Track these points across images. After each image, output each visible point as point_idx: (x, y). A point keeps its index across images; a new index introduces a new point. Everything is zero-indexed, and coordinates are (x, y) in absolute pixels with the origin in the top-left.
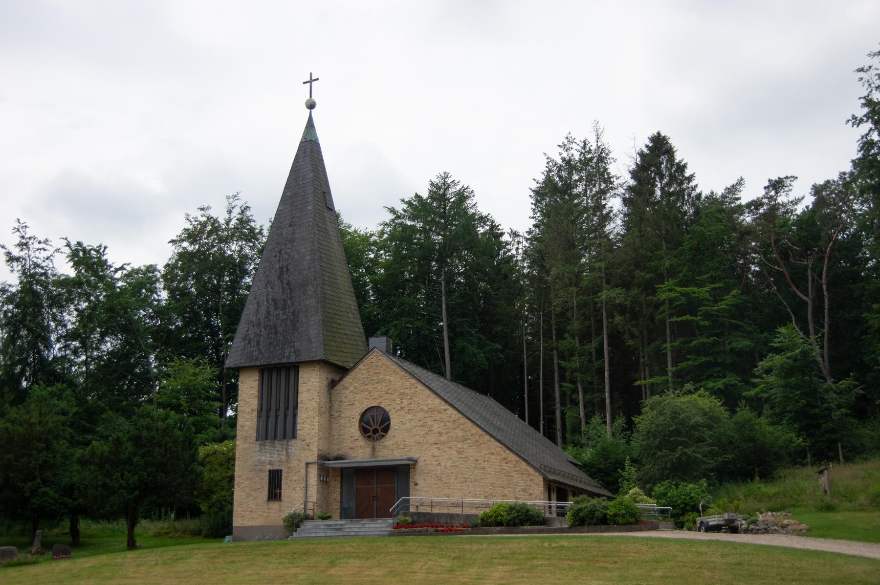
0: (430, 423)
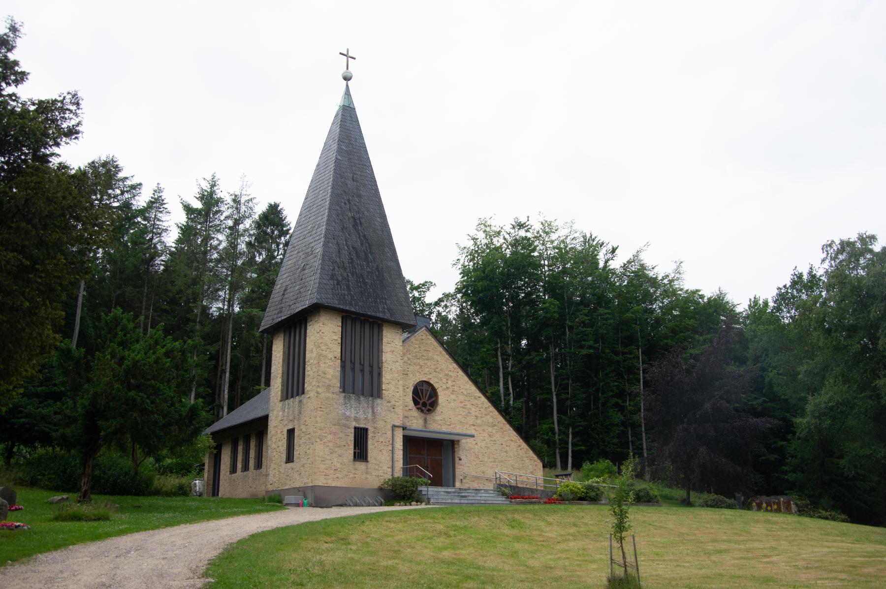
0: (469, 406)
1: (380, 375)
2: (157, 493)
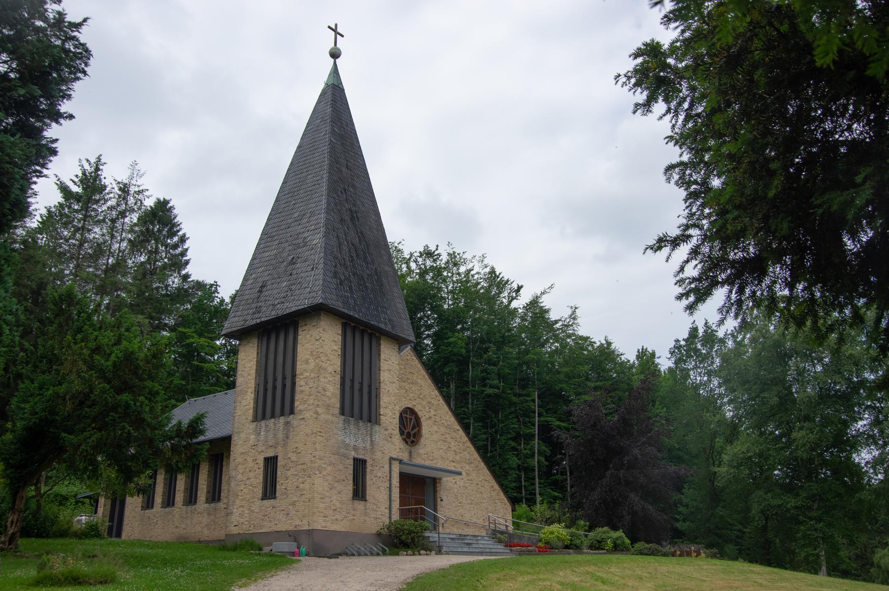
0: (449, 440)
1: (378, 396)
2: (64, 534)
